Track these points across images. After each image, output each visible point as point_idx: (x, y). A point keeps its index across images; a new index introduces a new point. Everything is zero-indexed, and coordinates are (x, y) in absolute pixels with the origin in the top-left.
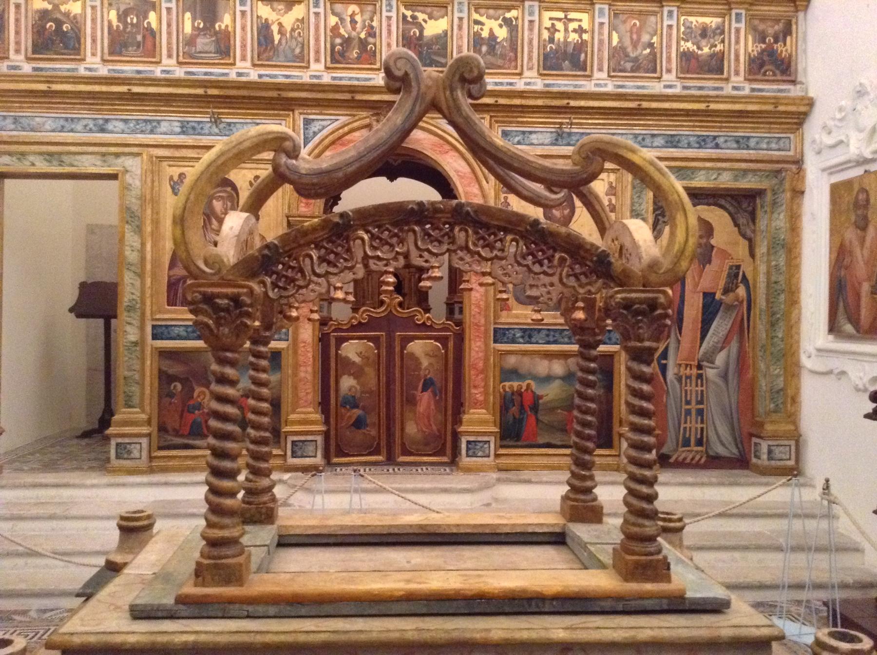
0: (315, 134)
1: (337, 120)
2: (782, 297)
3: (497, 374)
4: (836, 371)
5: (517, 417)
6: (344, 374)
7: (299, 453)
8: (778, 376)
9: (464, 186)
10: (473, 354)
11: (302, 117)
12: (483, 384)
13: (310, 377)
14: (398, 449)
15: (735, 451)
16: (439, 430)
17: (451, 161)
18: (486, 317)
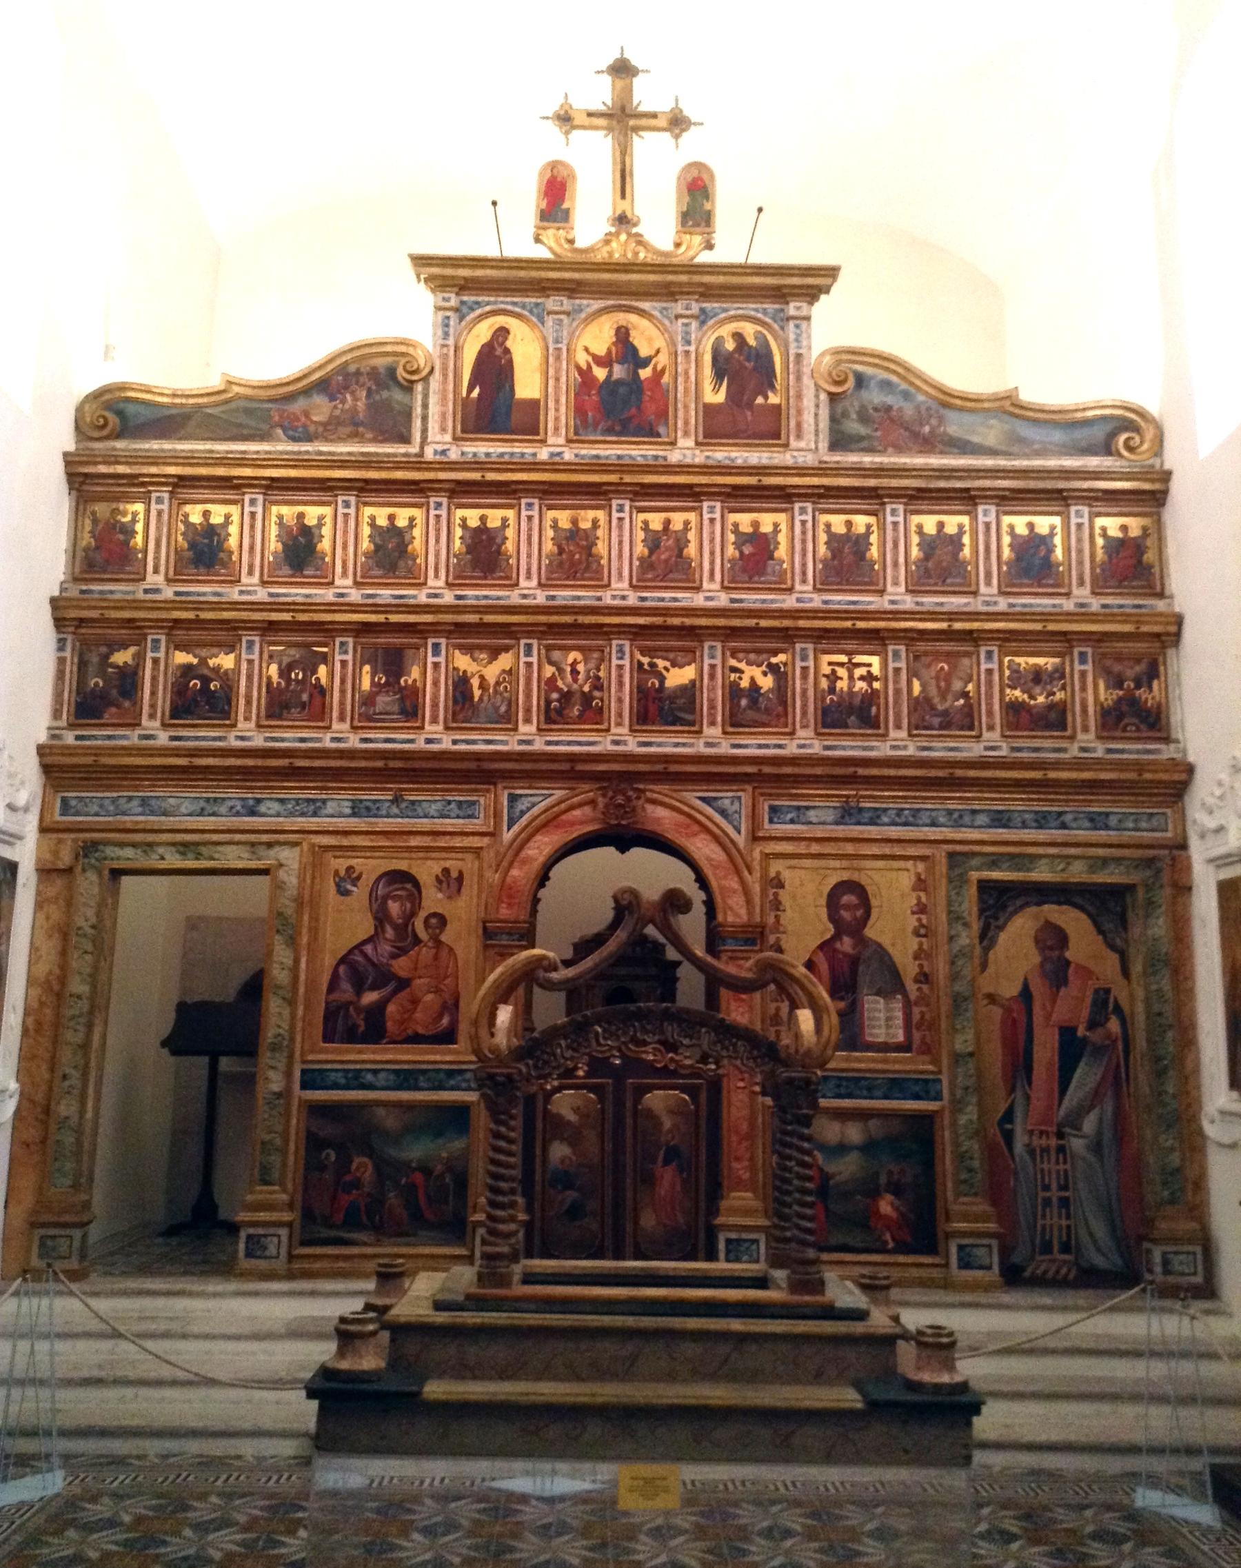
0: (523, 813)
1: (551, 795)
2: (1170, 1035)
8: (1172, 1149)
10: (734, 1110)
15: (1120, 1262)
17: (699, 845)
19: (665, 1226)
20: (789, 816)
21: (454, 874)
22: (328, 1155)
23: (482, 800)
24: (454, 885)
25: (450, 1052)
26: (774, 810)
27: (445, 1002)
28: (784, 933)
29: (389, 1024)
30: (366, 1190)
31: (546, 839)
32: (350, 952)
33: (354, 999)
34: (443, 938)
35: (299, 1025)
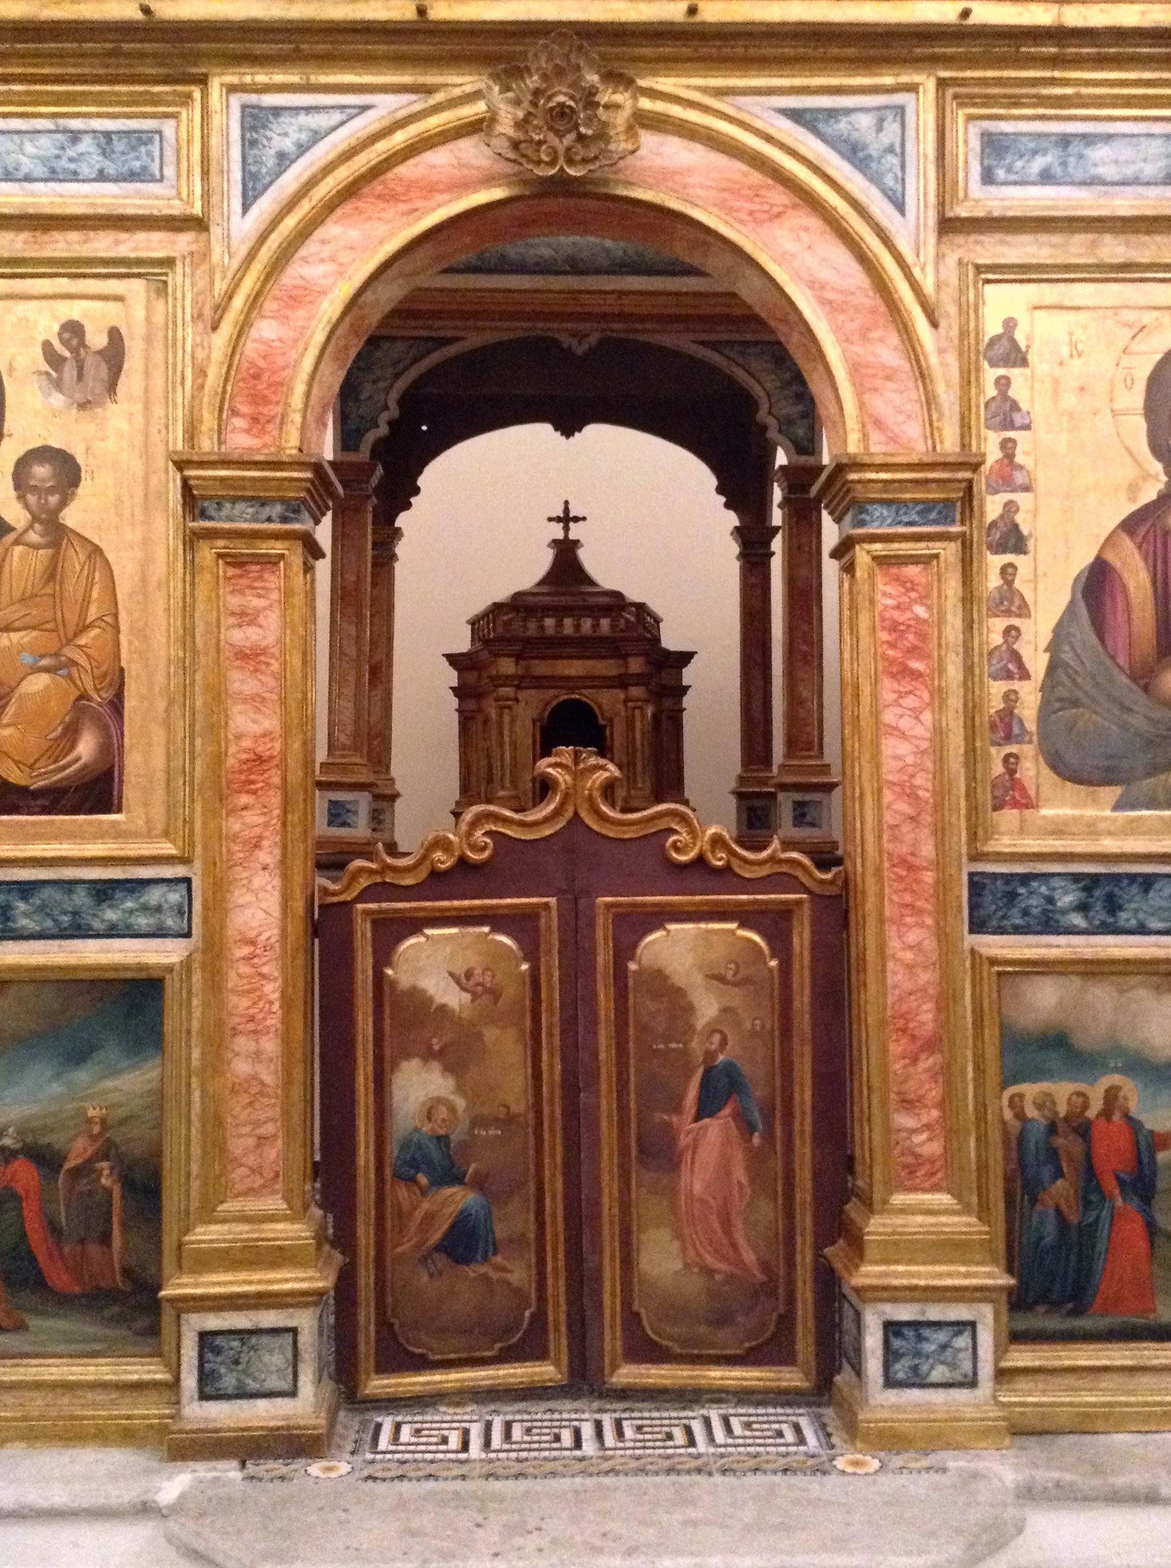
0: (284, 160)
1: (364, 108)
3: (991, 1051)
4: (376, 791)
5: (1074, 1219)
6: (408, 1056)
7: (229, 1382)
9: (845, 340)
10: (896, 976)
11: (236, 101)
12: (935, 1093)
13: (269, 1076)
14: (612, 1339)
16: (765, 1266)
17: (789, 246)
18: (940, 832)
19: (709, 1272)
20: (1038, 164)
21: (97, 339)
23: (168, 127)
24: (97, 371)
25: (100, 835)
26: (993, 145)
27: (83, 696)
28: (1027, 488)
31: (354, 234)
34: (71, 517)
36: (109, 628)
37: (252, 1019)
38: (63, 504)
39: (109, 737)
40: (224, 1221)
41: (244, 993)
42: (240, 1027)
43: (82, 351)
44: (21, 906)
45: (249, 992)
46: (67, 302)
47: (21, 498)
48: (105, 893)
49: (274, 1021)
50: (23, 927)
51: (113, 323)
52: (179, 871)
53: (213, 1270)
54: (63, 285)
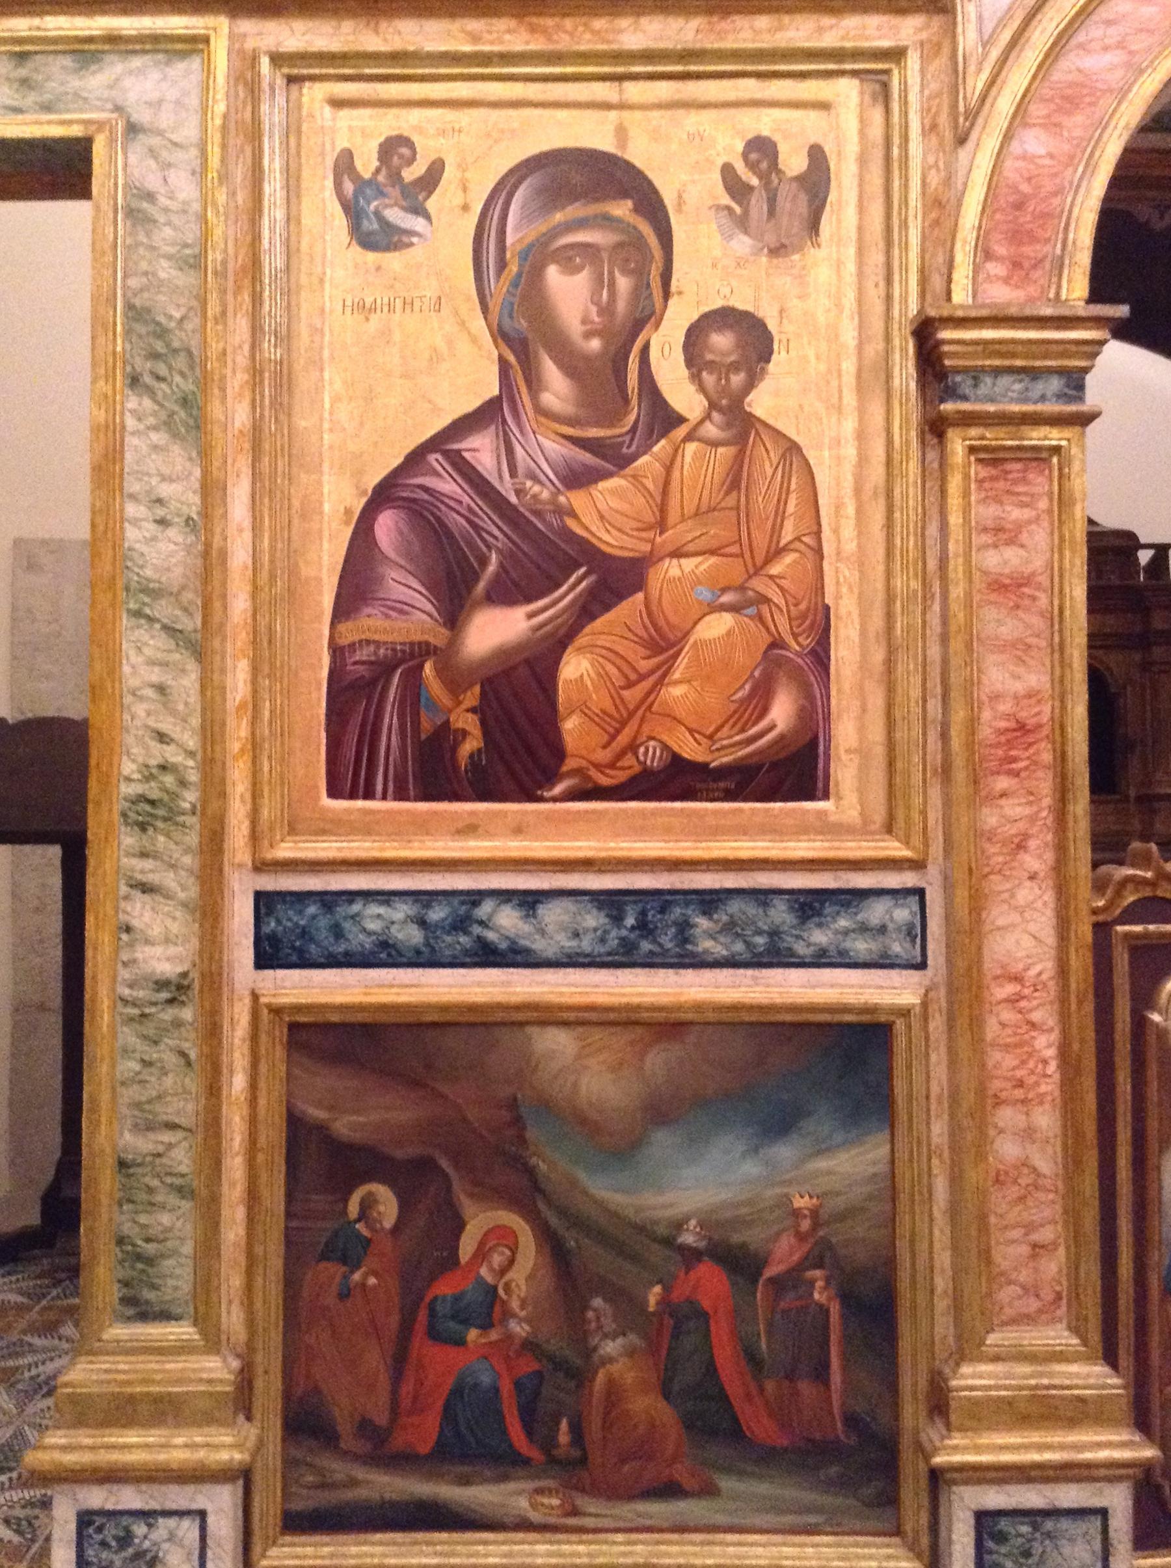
13: (1046, 1162)
21: (794, 162)
22: (367, 1205)
24: (793, 204)
25: (803, 830)
27: (777, 644)
29: (571, 725)
30: (519, 1329)
32: (416, 459)
33: (438, 636)
34: (760, 403)
35: (238, 732)
36: (809, 554)
37: (1020, 1084)
38: (750, 385)
39: (810, 698)
40: (996, 1359)
41: (1007, 1047)
42: (1003, 1095)
43: (774, 178)
44: (703, 923)
45: (1016, 1046)
46: (754, 112)
47: (696, 378)
48: (812, 908)
49: (1050, 1087)
50: (706, 951)
51: (812, 141)
52: (908, 879)
53: (993, 1427)
54: (748, 88)
